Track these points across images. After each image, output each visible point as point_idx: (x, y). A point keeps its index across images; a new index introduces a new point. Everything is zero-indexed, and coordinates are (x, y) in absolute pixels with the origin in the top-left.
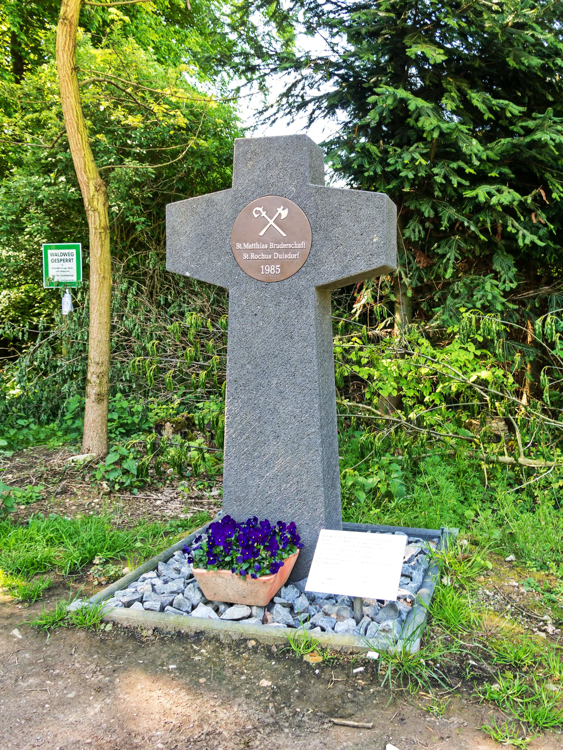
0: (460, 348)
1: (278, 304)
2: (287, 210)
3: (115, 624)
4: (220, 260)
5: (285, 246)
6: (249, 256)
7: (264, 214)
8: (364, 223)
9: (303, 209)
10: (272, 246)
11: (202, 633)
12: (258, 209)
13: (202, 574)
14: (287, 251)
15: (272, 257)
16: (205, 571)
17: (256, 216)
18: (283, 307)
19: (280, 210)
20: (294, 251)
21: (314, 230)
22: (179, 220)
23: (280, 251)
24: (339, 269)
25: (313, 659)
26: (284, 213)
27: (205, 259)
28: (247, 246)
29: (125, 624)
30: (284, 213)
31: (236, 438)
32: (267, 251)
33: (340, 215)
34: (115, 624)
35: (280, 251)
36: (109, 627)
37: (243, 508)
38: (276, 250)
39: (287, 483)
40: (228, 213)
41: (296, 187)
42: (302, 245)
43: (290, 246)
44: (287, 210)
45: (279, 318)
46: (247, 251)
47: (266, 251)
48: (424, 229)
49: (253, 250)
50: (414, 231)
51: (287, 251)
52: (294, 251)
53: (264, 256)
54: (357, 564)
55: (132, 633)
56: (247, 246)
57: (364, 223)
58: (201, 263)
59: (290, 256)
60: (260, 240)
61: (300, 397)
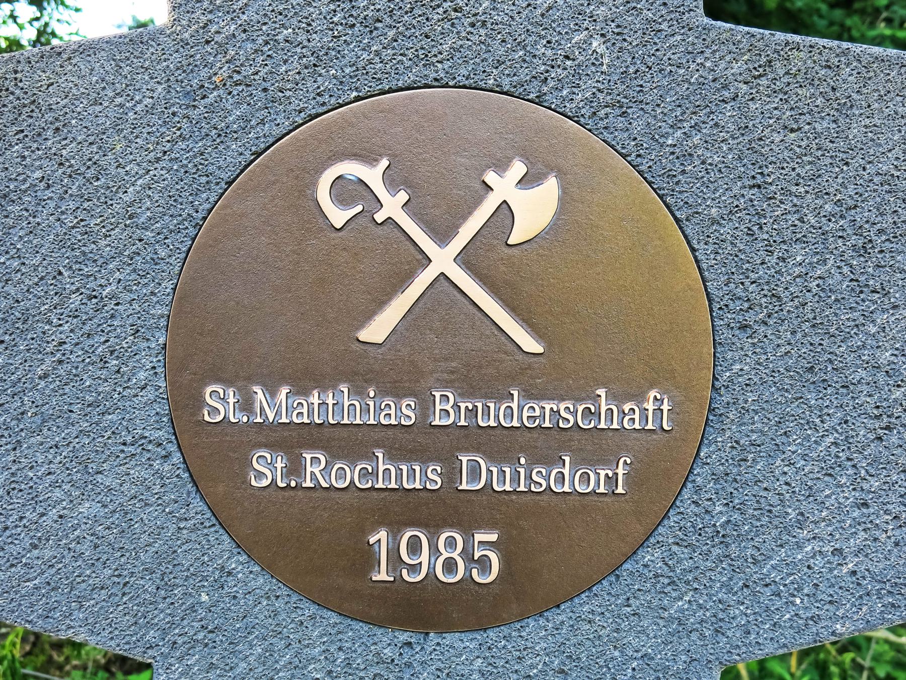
2: (550, 188)
4: (87, 487)
7: (392, 206)
10: (448, 409)
12: (351, 169)
14: (545, 445)
17: (338, 216)
19: (504, 185)
20: (593, 446)
23: (500, 444)
35: (500, 444)
41: (616, 36)
43: (570, 413)
44: (550, 188)
51: (545, 445)
52: (593, 446)
53: (388, 473)
56: (278, 406)
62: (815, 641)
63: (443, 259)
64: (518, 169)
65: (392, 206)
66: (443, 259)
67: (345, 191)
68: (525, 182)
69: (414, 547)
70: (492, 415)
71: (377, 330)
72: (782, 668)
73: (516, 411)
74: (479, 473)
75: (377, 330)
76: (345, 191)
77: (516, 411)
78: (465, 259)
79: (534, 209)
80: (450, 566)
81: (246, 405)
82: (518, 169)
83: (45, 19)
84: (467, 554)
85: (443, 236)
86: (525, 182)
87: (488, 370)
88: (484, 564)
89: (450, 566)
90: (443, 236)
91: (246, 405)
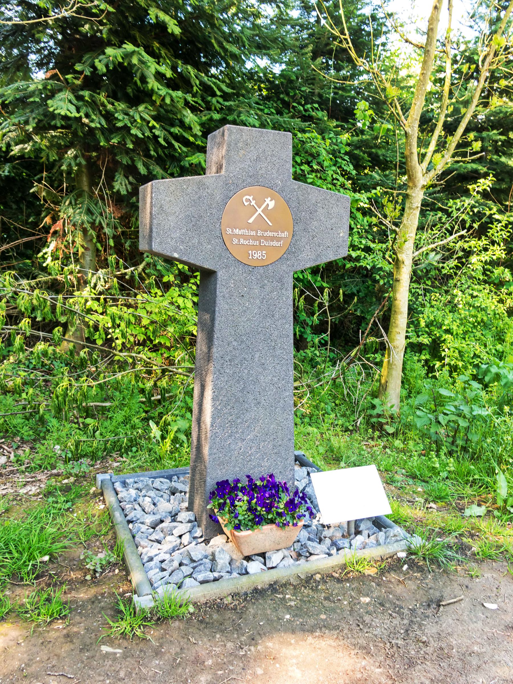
0: (179, 296)
1: (262, 287)
2: (273, 201)
3: (195, 604)
4: (209, 243)
5: (271, 234)
6: (239, 241)
7: (253, 203)
8: (333, 221)
9: (287, 202)
10: (260, 233)
11: (276, 583)
12: (248, 197)
13: (249, 535)
14: (272, 239)
15: (260, 243)
16: (249, 532)
17: (246, 204)
18: (268, 289)
19: (268, 201)
20: (278, 239)
21: (296, 221)
22: (168, 199)
23: (266, 238)
24: (313, 257)
25: (372, 571)
26: (272, 204)
27: (196, 241)
28: (237, 231)
29: (203, 600)
30: (272, 204)
31: (222, 409)
32: (256, 238)
33: (317, 211)
34: (195, 604)
35: (266, 238)
36: (191, 609)
37: (227, 470)
38: (263, 237)
39: (264, 441)
40: (218, 197)
41: (282, 181)
42: (285, 234)
43: (275, 234)
44: (273, 201)
45: (263, 299)
46: (238, 236)
47: (256, 238)
48: (130, 183)
49: (243, 236)
50: (121, 183)
51: (272, 239)
52: (278, 239)
53: (251, 242)
54: (348, 492)
55: (217, 605)
56: (237, 231)
57: (333, 221)
58: (190, 244)
59: (275, 243)
60: (249, 227)
61: (278, 367)
66: (260, 211)
70: (267, 234)
71: (250, 221)
72: (399, 296)
74: (264, 243)
75: (250, 221)
85: (259, 208)
90: (259, 208)
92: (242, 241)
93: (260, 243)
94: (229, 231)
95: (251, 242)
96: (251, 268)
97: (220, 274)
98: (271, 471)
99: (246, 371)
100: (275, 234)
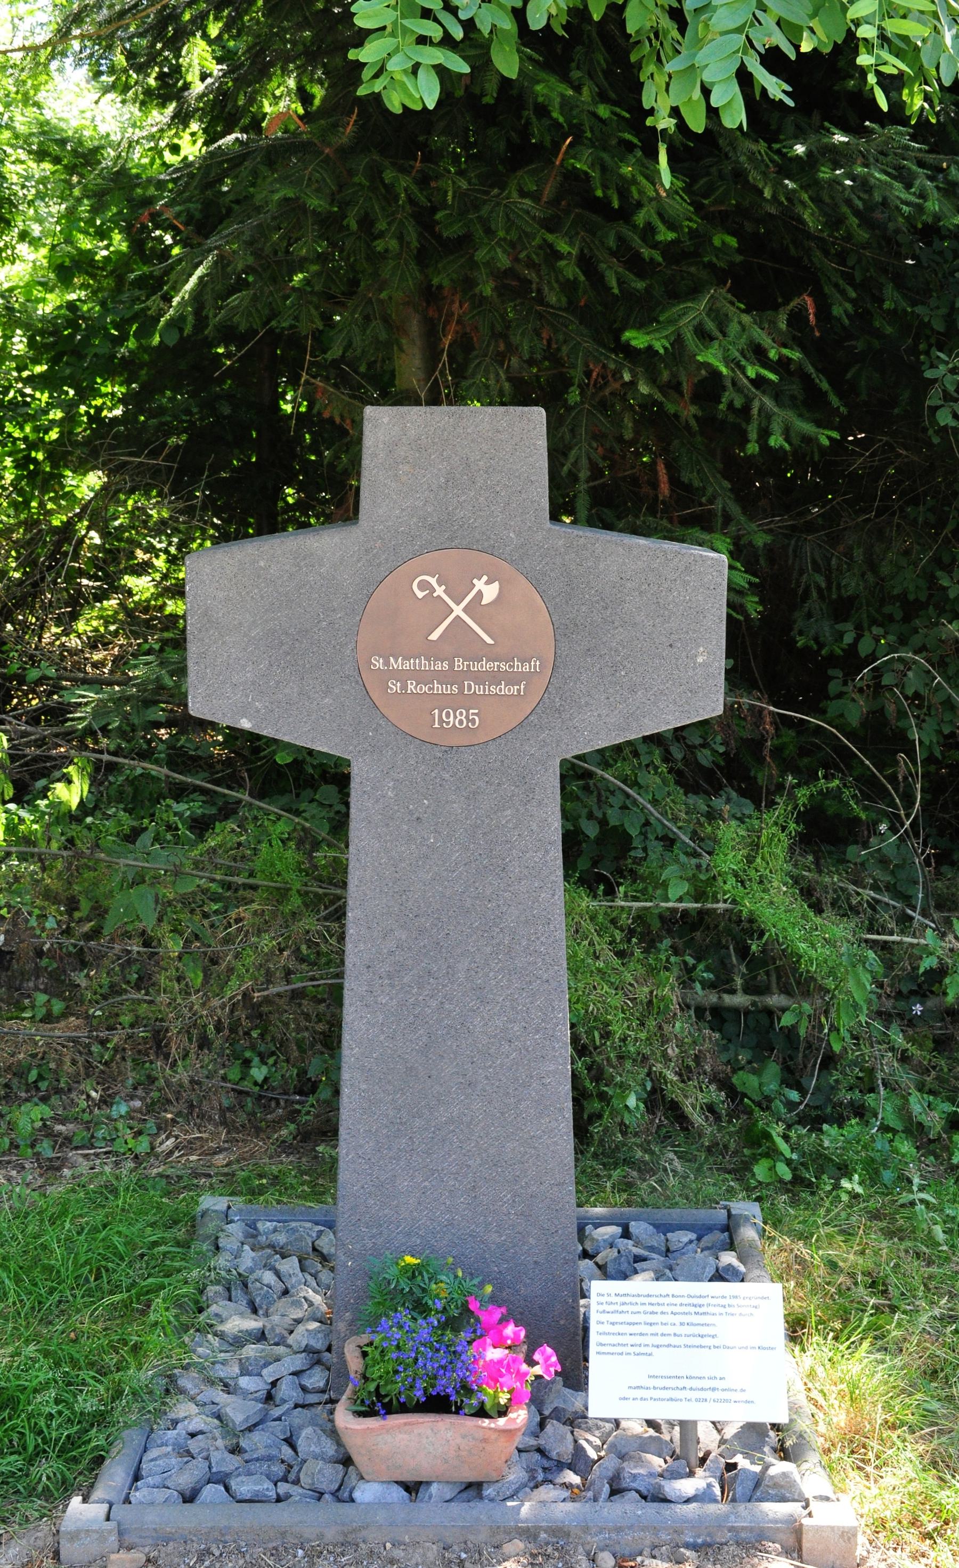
2: (496, 585)
6: (404, 687)
7: (440, 591)
10: (459, 664)
14: (495, 678)
15: (461, 689)
17: (420, 595)
19: (479, 584)
22: (221, 595)
23: (479, 678)
26: (490, 592)
28: (397, 664)
35: (479, 678)
38: (468, 674)
41: (519, 534)
43: (504, 667)
44: (496, 585)
46: (398, 676)
49: (421, 677)
51: (495, 678)
52: (512, 679)
56: (397, 664)
59: (503, 689)
60: (433, 651)
62: (832, 973)
63: (458, 610)
64: (485, 578)
65: (440, 591)
66: (458, 610)
67: (424, 585)
68: (487, 583)
69: (448, 715)
70: (476, 667)
71: (434, 636)
73: (486, 666)
75: (434, 636)
76: (424, 585)
77: (486, 666)
78: (465, 610)
79: (490, 592)
80: (461, 722)
81: (387, 663)
82: (485, 578)
83: (149, 303)
84: (467, 717)
85: (465, 610)
86: (487, 583)
87: (476, 651)
88: (473, 721)
89: (461, 722)
90: (465, 610)
91: (387, 663)
92: (411, 687)
93: (461, 689)
94: (378, 663)
95: (438, 688)
96: (446, 751)
97: (359, 773)
98: (556, 527)
99: (434, 1004)
100: (504, 667)
